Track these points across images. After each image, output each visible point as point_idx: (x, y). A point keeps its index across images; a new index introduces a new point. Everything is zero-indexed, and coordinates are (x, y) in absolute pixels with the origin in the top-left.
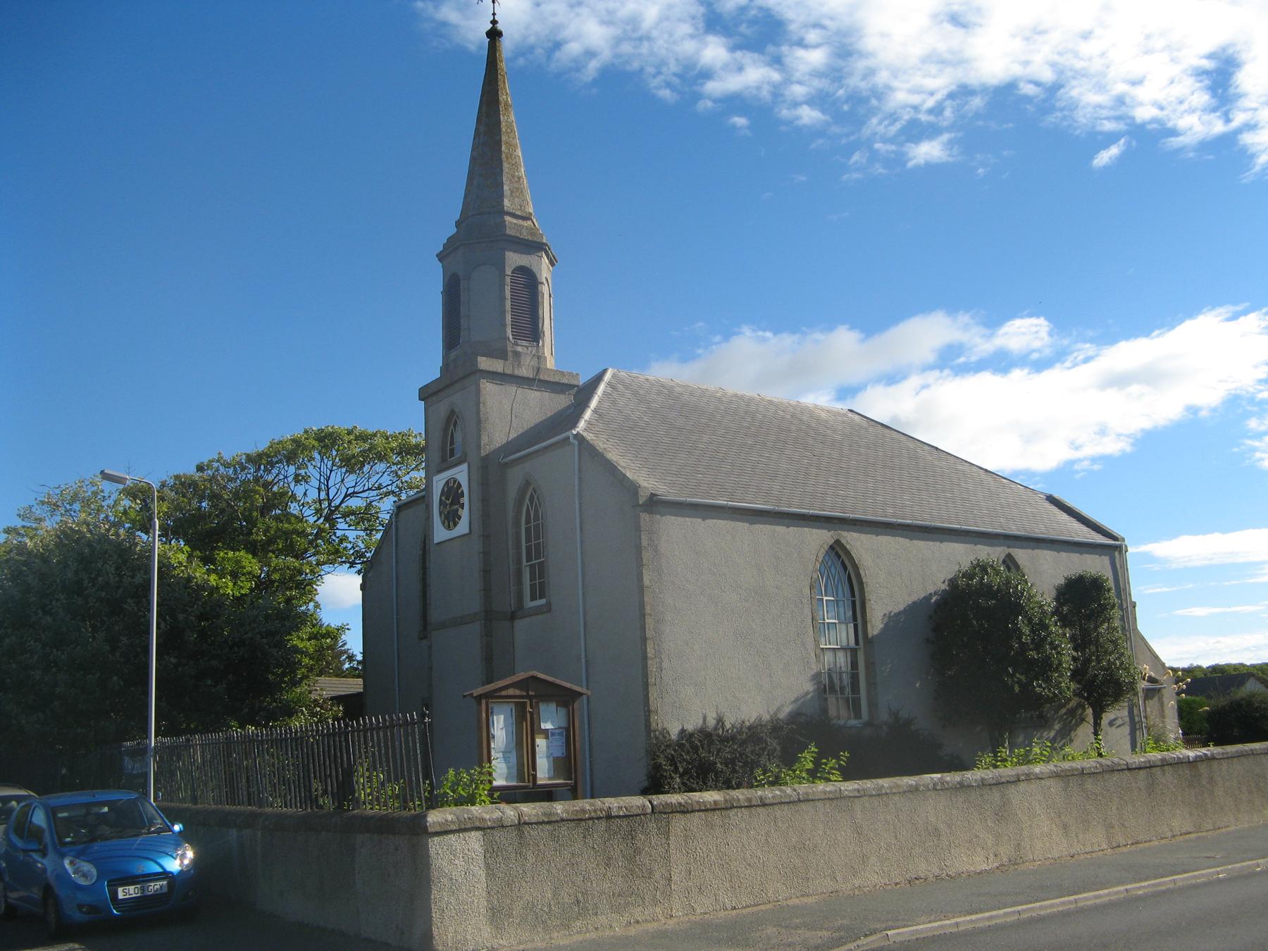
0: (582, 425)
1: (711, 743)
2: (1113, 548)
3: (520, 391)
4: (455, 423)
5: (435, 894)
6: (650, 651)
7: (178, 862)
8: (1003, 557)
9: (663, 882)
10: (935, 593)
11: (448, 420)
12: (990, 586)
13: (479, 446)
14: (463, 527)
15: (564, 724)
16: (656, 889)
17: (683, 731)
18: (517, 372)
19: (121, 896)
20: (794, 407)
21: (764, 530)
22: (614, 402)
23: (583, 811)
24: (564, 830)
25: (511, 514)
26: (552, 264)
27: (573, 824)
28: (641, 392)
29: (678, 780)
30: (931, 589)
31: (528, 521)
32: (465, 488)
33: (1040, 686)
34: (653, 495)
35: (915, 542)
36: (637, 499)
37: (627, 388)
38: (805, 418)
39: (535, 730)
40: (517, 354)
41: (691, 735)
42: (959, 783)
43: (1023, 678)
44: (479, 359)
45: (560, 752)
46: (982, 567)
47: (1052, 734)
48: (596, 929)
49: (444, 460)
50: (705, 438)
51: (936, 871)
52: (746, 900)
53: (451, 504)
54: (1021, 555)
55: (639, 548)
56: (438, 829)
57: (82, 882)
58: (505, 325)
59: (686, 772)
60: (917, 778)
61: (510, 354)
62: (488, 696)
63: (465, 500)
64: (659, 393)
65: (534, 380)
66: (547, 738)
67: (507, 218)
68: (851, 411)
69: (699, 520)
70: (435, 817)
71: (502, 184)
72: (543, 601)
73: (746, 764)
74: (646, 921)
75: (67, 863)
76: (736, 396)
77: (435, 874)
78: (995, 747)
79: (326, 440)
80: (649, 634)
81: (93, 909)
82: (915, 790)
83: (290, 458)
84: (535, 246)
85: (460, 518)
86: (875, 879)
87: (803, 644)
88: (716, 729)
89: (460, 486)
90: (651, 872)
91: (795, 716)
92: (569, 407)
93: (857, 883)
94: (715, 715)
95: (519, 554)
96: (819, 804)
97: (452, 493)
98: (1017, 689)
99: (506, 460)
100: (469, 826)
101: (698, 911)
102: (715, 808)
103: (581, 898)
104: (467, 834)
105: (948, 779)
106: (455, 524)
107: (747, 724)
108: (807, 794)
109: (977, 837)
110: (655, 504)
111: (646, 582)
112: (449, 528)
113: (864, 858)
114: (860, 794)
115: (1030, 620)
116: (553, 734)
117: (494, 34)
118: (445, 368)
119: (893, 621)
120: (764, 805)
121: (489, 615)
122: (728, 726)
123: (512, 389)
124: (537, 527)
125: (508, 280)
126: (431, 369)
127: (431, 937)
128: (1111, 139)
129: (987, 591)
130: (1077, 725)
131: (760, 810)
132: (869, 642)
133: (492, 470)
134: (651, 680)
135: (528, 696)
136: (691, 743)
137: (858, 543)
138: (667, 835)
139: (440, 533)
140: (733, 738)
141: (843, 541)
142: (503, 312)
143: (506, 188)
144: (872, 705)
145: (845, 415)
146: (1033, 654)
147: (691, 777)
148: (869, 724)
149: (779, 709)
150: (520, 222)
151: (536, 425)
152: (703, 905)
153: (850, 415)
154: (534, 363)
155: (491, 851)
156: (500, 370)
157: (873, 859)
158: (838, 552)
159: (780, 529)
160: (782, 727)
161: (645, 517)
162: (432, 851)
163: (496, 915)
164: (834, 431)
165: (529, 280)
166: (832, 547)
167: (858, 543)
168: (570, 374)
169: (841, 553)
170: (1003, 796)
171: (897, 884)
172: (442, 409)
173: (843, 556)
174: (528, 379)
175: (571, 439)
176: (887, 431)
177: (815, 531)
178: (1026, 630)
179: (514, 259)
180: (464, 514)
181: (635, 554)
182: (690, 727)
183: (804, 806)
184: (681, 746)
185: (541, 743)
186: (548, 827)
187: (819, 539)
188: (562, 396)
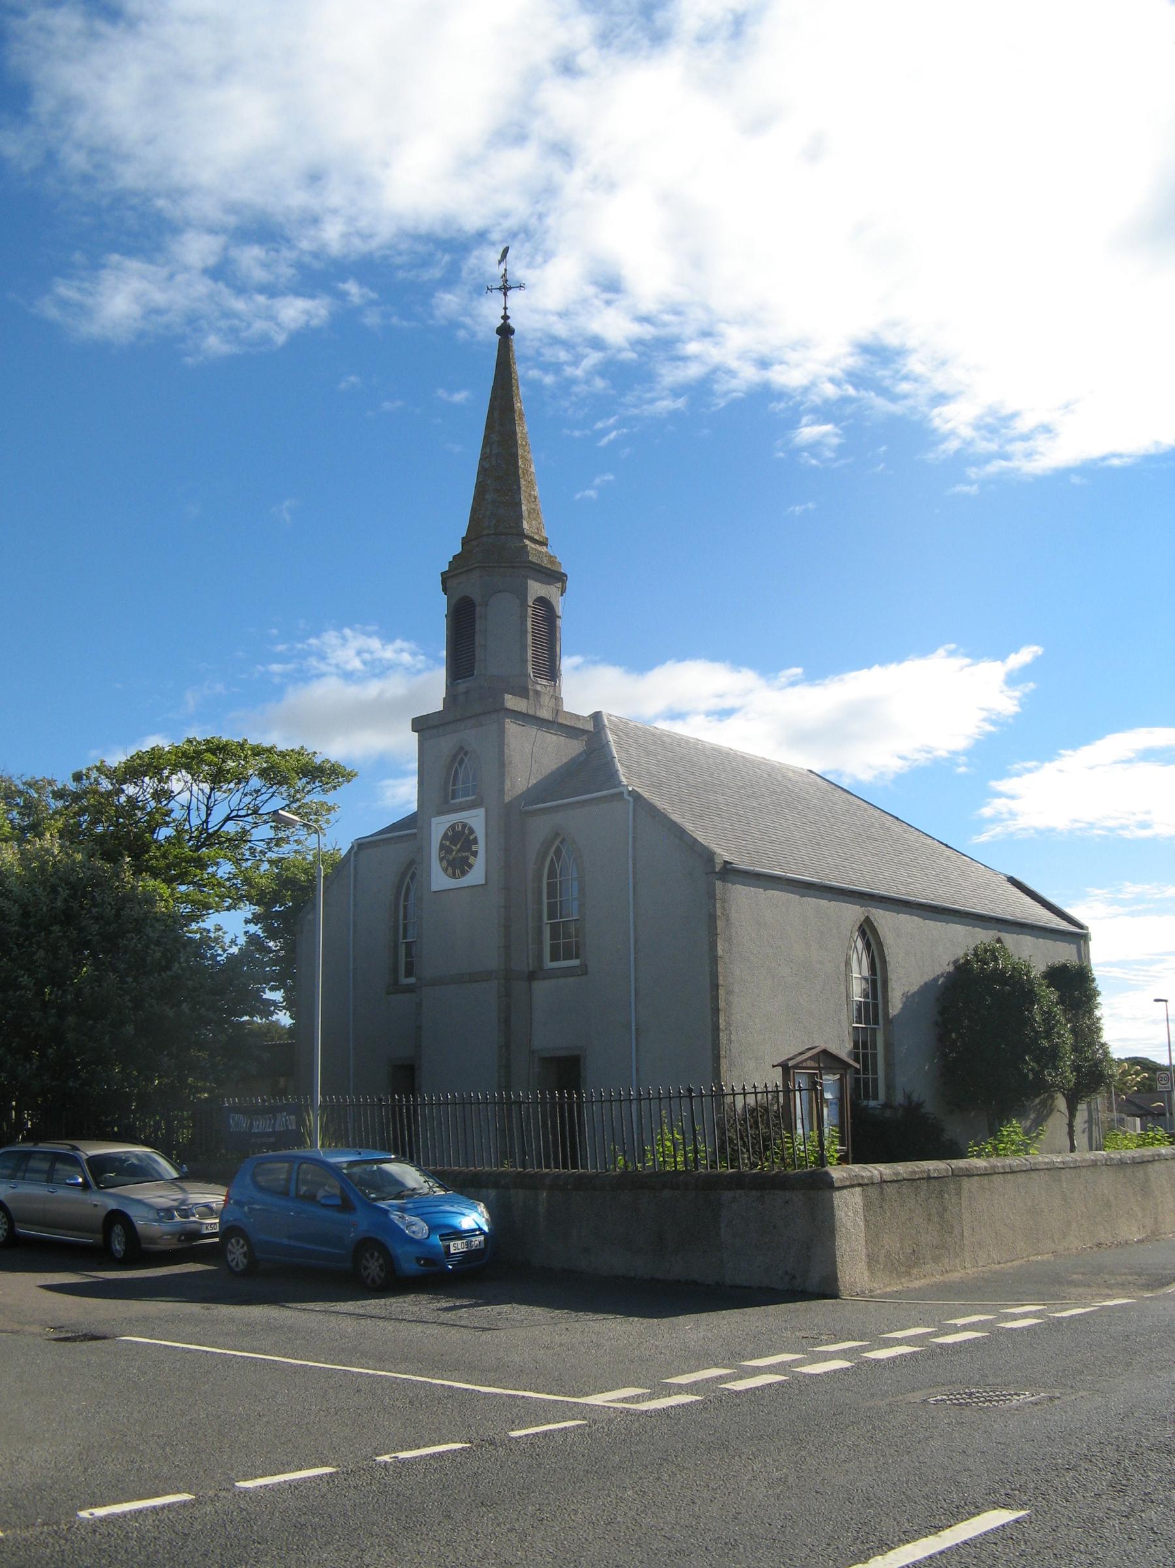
2: (1078, 936)
4: (462, 761)
10: (942, 975)
11: (455, 756)
12: (1003, 972)
13: (501, 791)
14: (476, 875)
15: (838, 1095)
33: (1050, 1075)
35: (951, 925)
40: (537, 693)
44: (507, 697)
54: (1009, 939)
55: (712, 918)
58: (526, 661)
61: (531, 693)
63: (481, 847)
67: (527, 542)
71: (519, 504)
72: (575, 962)
77: (838, 1224)
78: (993, 1132)
80: (722, 1004)
84: (556, 577)
85: (470, 866)
89: (472, 831)
92: (581, 754)
95: (540, 912)
96: (1042, 1173)
97: (460, 839)
98: (1031, 1076)
106: (464, 873)
110: (729, 872)
111: (720, 952)
112: (454, 876)
115: (1041, 1008)
117: (505, 331)
118: (451, 698)
119: (909, 999)
120: (1012, 1172)
123: (532, 731)
127: (836, 1279)
130: (1048, 1115)
131: (1009, 1176)
132: (888, 1021)
133: (513, 818)
134: (722, 1053)
137: (884, 919)
139: (439, 879)
142: (524, 647)
143: (524, 508)
144: (890, 1087)
148: (886, 1105)
151: (553, 773)
153: (811, 775)
154: (552, 703)
157: (1074, 1225)
159: (824, 903)
161: (718, 883)
163: (871, 1260)
165: (548, 614)
167: (884, 919)
170: (1145, 1173)
174: (548, 721)
175: (626, 796)
176: (848, 796)
179: (536, 589)
181: (709, 922)
186: (896, 1185)
187: (853, 913)
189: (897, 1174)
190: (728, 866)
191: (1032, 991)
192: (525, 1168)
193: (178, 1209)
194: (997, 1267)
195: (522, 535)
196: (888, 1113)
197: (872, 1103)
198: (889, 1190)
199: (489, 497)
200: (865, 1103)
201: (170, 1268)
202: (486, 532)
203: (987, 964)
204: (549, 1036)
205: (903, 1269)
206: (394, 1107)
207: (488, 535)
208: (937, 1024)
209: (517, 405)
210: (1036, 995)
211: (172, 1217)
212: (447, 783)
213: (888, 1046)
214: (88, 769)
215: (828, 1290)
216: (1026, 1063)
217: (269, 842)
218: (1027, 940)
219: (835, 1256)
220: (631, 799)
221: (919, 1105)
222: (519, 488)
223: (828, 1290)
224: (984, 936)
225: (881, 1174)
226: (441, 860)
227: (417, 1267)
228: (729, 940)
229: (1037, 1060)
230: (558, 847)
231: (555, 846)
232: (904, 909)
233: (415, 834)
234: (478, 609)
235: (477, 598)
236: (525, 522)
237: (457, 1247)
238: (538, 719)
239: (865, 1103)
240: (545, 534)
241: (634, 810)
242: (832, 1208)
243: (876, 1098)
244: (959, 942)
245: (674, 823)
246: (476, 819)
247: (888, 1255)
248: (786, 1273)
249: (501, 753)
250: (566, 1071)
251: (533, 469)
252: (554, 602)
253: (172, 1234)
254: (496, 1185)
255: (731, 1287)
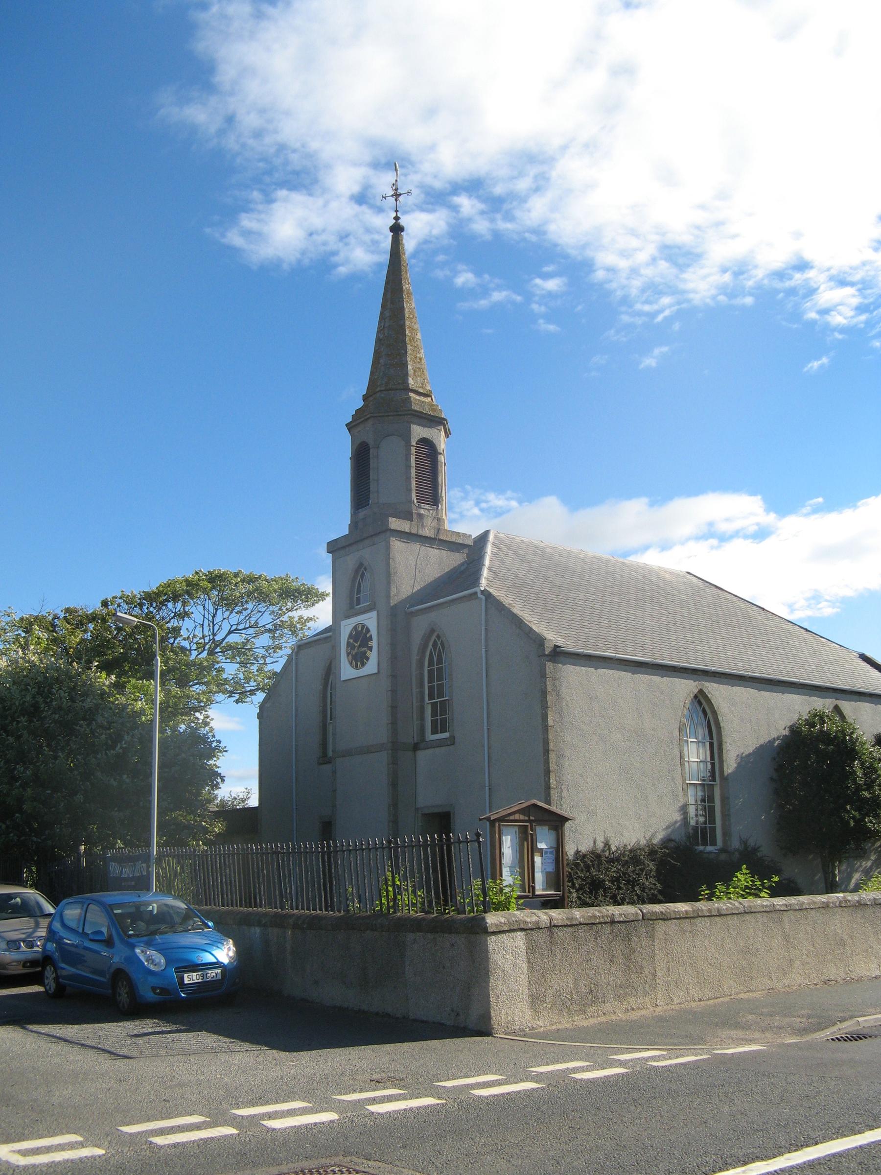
0: (483, 582)
1: (600, 863)
3: (423, 548)
4: (363, 574)
5: (492, 982)
6: (553, 782)
7: (224, 953)
8: (832, 707)
9: (650, 977)
10: (778, 738)
11: (357, 571)
12: (827, 734)
13: (388, 597)
14: (371, 667)
16: (646, 982)
17: (577, 852)
18: (421, 532)
19: (186, 982)
20: (642, 568)
21: (644, 679)
22: (502, 561)
23: (595, 917)
24: (581, 930)
25: (415, 658)
26: (447, 436)
27: (587, 927)
28: (521, 552)
29: (574, 895)
30: (774, 735)
31: (431, 663)
32: (374, 632)
33: (871, 822)
34: (556, 647)
36: (544, 650)
37: (509, 549)
38: (654, 579)
39: (533, 849)
40: (420, 516)
41: (584, 856)
42: (858, 902)
43: (857, 814)
44: (390, 519)
45: (551, 868)
46: (822, 718)
47: (869, 863)
48: (604, 1014)
49: (351, 607)
50: (582, 596)
51: (843, 976)
52: (709, 994)
53: (360, 647)
54: (847, 706)
55: (544, 693)
56: (495, 929)
57: (152, 967)
58: (411, 490)
59: (581, 888)
60: (826, 896)
61: (415, 516)
62: (501, 819)
63: (374, 643)
64: (535, 554)
65: (435, 539)
66: (542, 856)
67: (412, 395)
68: (689, 573)
69: (592, 669)
70: (492, 919)
71: (405, 365)
72: (446, 735)
73: (628, 882)
74: (639, 1008)
75: (138, 951)
76: (595, 557)
77: (492, 966)
79: (216, 579)
80: (552, 767)
81: (164, 991)
82: (826, 906)
83: (175, 598)
84: (436, 421)
85: (368, 659)
86: (799, 980)
87: (673, 779)
88: (603, 851)
89: (368, 630)
90: (642, 967)
91: (666, 842)
92: (462, 564)
93: (787, 982)
94: (603, 840)
95: (422, 694)
96: (759, 916)
97: (360, 637)
98: (852, 823)
99: (413, 609)
100: (516, 927)
101: (676, 1001)
102: (686, 917)
103: (593, 989)
104: (514, 934)
105: (849, 898)
106: (363, 664)
107: (629, 848)
108: (750, 907)
109: (871, 947)
110: (558, 654)
111: (550, 723)
112: (356, 667)
113: (791, 961)
114: (788, 909)
115: (862, 764)
116: (546, 853)
118: (354, 525)
119: (744, 761)
120: (720, 915)
121: (396, 747)
122: (614, 848)
123: (416, 547)
124: (440, 670)
125: (413, 450)
126: (340, 524)
127: (490, 1018)
128: (780, 292)
129: (825, 737)
131: (717, 919)
132: (724, 779)
133: (399, 618)
135: (529, 821)
136: (585, 862)
137: (717, 692)
138: (652, 937)
139: (347, 671)
140: (618, 860)
141: (705, 691)
142: (409, 478)
143: (410, 367)
144: (726, 834)
145: (684, 577)
146: (866, 794)
147: (584, 892)
148: (723, 850)
149: (653, 835)
150: (422, 398)
151: (435, 580)
152: (679, 996)
153: (688, 576)
155: (532, 949)
156: (407, 530)
157: (797, 963)
158: (701, 700)
159: (656, 679)
160: (656, 851)
161: (549, 665)
162: (490, 947)
163: (535, 1001)
164: (679, 591)
165: (429, 450)
166: (696, 697)
167: (717, 692)
168: (464, 535)
169: (702, 701)
171: (816, 984)
172: (350, 561)
173: (704, 704)
174: (430, 538)
175: (479, 595)
176: (720, 592)
177: (683, 681)
178: (860, 773)
179: (418, 432)
180: (373, 656)
181: (540, 698)
182: (583, 849)
183: (748, 917)
184: (577, 865)
185: (538, 859)
186: (570, 929)
187: (686, 687)
188: (457, 554)
189: (572, 919)
190: (558, 650)
191: (853, 750)
192: (282, 908)
193: (24, 942)
194: (694, 1004)
195: (408, 389)
196: (723, 857)
197: (710, 848)
198: (559, 934)
199: (382, 361)
200: (701, 848)
201: (18, 989)
202: (378, 389)
203: (814, 727)
204: (429, 797)
205: (576, 1008)
206: (323, 853)
207: (381, 391)
208: (772, 779)
209: (406, 287)
210: (857, 753)
211: (19, 947)
212: (352, 592)
213: (725, 799)
214: (113, 598)
215: (483, 1029)
216: (848, 812)
217: (267, 648)
218: (866, 708)
219: (488, 996)
220: (483, 598)
221: (755, 850)
222: (406, 352)
223: (483, 1029)
224: (823, 704)
225: (551, 919)
226: (348, 654)
227: (152, 994)
228: (560, 713)
229: (859, 809)
230: (435, 641)
231: (432, 640)
232: (737, 682)
233: (330, 637)
234: (371, 451)
235: (371, 443)
236: (410, 379)
237: (191, 978)
238: (421, 536)
239: (701, 848)
240: (429, 388)
241: (486, 607)
242: (487, 951)
243: (714, 843)
244: (792, 710)
245: (515, 616)
246: (370, 620)
247: (558, 995)
248: (453, 1011)
249: (388, 565)
250: (442, 821)
251: (419, 336)
252: (435, 442)
253: (18, 962)
254: (259, 924)
255: (415, 1020)
